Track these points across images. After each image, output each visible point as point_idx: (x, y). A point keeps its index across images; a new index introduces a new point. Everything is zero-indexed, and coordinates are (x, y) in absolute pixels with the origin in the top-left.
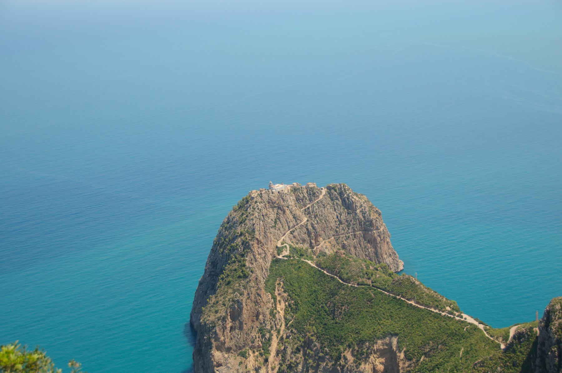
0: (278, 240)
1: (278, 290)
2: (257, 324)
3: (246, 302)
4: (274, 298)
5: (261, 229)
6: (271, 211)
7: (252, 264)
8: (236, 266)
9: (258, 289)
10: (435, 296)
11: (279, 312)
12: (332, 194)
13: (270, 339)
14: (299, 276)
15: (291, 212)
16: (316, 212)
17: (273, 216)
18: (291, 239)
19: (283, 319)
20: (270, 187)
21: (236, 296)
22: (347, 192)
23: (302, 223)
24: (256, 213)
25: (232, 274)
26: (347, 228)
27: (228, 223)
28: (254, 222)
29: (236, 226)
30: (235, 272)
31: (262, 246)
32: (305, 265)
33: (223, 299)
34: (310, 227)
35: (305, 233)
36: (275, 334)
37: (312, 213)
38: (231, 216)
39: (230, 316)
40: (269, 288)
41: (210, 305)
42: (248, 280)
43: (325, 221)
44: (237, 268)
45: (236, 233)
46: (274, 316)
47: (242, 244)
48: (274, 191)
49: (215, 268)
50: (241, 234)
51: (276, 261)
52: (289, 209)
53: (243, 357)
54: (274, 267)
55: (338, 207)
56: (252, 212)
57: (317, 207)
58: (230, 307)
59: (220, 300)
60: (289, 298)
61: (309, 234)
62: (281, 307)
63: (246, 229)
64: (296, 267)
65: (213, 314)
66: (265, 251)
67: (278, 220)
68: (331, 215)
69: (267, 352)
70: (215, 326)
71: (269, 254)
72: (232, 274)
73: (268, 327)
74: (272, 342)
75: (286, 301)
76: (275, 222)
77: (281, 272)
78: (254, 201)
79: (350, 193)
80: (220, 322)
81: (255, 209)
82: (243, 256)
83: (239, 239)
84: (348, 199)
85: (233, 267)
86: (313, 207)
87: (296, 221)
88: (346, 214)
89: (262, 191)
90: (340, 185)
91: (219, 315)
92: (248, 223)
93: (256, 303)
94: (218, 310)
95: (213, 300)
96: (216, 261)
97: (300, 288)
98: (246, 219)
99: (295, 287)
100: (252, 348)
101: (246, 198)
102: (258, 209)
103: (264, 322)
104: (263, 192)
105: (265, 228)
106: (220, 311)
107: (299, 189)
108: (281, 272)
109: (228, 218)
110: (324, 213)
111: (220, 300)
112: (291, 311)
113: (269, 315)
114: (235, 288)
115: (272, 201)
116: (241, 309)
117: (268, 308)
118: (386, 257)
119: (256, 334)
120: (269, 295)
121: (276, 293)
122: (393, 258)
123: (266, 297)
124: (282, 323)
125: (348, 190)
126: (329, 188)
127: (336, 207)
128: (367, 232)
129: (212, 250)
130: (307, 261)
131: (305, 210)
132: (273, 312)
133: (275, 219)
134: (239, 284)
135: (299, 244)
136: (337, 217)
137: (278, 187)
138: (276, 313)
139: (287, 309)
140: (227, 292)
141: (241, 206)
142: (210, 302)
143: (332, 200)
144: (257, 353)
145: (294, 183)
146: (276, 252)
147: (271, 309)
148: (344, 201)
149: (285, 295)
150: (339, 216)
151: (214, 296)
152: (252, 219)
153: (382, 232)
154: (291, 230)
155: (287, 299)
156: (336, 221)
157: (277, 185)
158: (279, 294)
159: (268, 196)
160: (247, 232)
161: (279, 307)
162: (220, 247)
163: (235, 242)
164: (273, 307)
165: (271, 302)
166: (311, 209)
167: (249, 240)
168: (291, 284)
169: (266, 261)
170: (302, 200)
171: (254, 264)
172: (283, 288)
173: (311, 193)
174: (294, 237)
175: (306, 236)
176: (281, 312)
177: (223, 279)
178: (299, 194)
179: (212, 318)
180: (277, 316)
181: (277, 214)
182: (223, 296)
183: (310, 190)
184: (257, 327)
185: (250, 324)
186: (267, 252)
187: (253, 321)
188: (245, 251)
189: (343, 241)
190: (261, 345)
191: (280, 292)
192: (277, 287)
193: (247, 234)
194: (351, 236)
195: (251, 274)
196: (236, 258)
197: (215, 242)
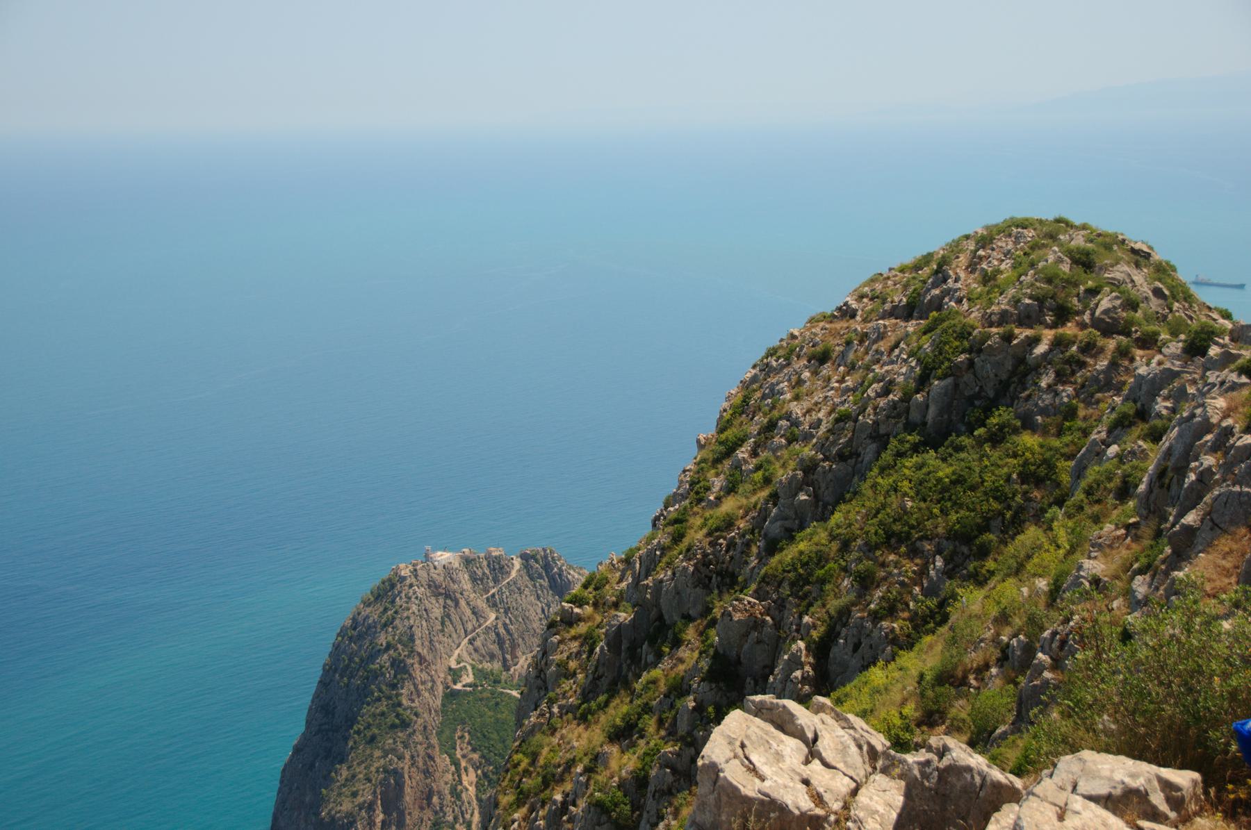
0: (450, 657)
1: (462, 749)
2: (428, 814)
4: (456, 763)
5: (424, 636)
6: (434, 602)
7: (413, 701)
8: (383, 706)
9: (428, 747)
11: (467, 790)
12: (532, 567)
14: (497, 720)
15: (468, 604)
16: (507, 603)
17: (437, 612)
18: (470, 654)
19: (475, 802)
20: (427, 557)
21: (390, 761)
23: (488, 623)
25: (377, 721)
27: (355, 629)
28: (412, 622)
29: (376, 632)
30: (383, 718)
31: (426, 668)
32: (506, 699)
33: (365, 769)
34: (502, 631)
35: (494, 642)
38: (359, 614)
39: (381, 799)
40: (445, 746)
41: (338, 784)
42: (410, 730)
43: (523, 620)
44: (385, 709)
45: (377, 644)
47: (392, 665)
48: (436, 563)
49: (330, 716)
50: (389, 647)
51: (451, 695)
54: (450, 706)
56: (405, 605)
57: (508, 594)
58: (380, 783)
59: (360, 773)
60: (483, 761)
61: (500, 642)
62: (469, 779)
63: (397, 637)
64: (491, 704)
65: (348, 799)
66: (431, 677)
67: (446, 619)
70: (355, 822)
71: (439, 683)
72: (377, 721)
73: (450, 818)
74: (799, 722)
75: (478, 768)
76: (443, 623)
77: (464, 715)
78: (408, 584)
79: (563, 565)
80: (363, 813)
81: (410, 598)
82: (394, 686)
83: (385, 657)
84: (560, 575)
85: (376, 708)
86: (502, 593)
87: (478, 620)
89: (417, 565)
90: (545, 550)
91: (360, 799)
92: (400, 626)
93: (427, 773)
94: (358, 791)
95: (345, 773)
96: (331, 704)
97: (504, 742)
98: (394, 619)
99: (493, 739)
101: (390, 580)
102: (417, 598)
103: (441, 808)
104: (418, 567)
105: (430, 633)
106: (361, 792)
107: (474, 560)
108: (464, 715)
109: (354, 619)
111: (360, 773)
112: (489, 785)
113: (449, 796)
114: (387, 747)
115: (434, 582)
116: (400, 785)
117: (446, 783)
121: (459, 754)
123: (443, 761)
124: (473, 809)
125: (559, 560)
126: (525, 557)
127: (539, 592)
129: (320, 682)
130: (509, 691)
131: (488, 599)
132: (456, 790)
134: (394, 739)
135: (484, 663)
136: (543, 611)
137: (443, 557)
138: (462, 792)
139: (482, 782)
140: (371, 756)
141: (379, 595)
142: (339, 778)
143: (532, 579)
145: (464, 550)
146: (450, 678)
147: (452, 785)
148: (554, 579)
149: (476, 756)
150: (546, 609)
151: (344, 767)
152: (408, 618)
154: (469, 637)
155: (480, 764)
156: (541, 619)
157: (439, 553)
158: (464, 756)
160: (400, 641)
162: (342, 676)
163: (378, 661)
164: (454, 780)
167: (405, 656)
168: (484, 736)
169: (434, 696)
170: (482, 580)
171: (416, 701)
172: (469, 743)
173: (497, 567)
174: (476, 650)
175: (495, 648)
176: (470, 788)
177: (358, 732)
178: (475, 569)
179: (347, 806)
180: (464, 795)
181: (444, 607)
182: (364, 765)
183: (494, 562)
184: (429, 819)
185: (416, 813)
186: (435, 678)
187: (422, 808)
188: (399, 677)
191: (465, 751)
192: (458, 744)
193: (399, 646)
195: (415, 718)
196: (380, 690)
197: (327, 667)
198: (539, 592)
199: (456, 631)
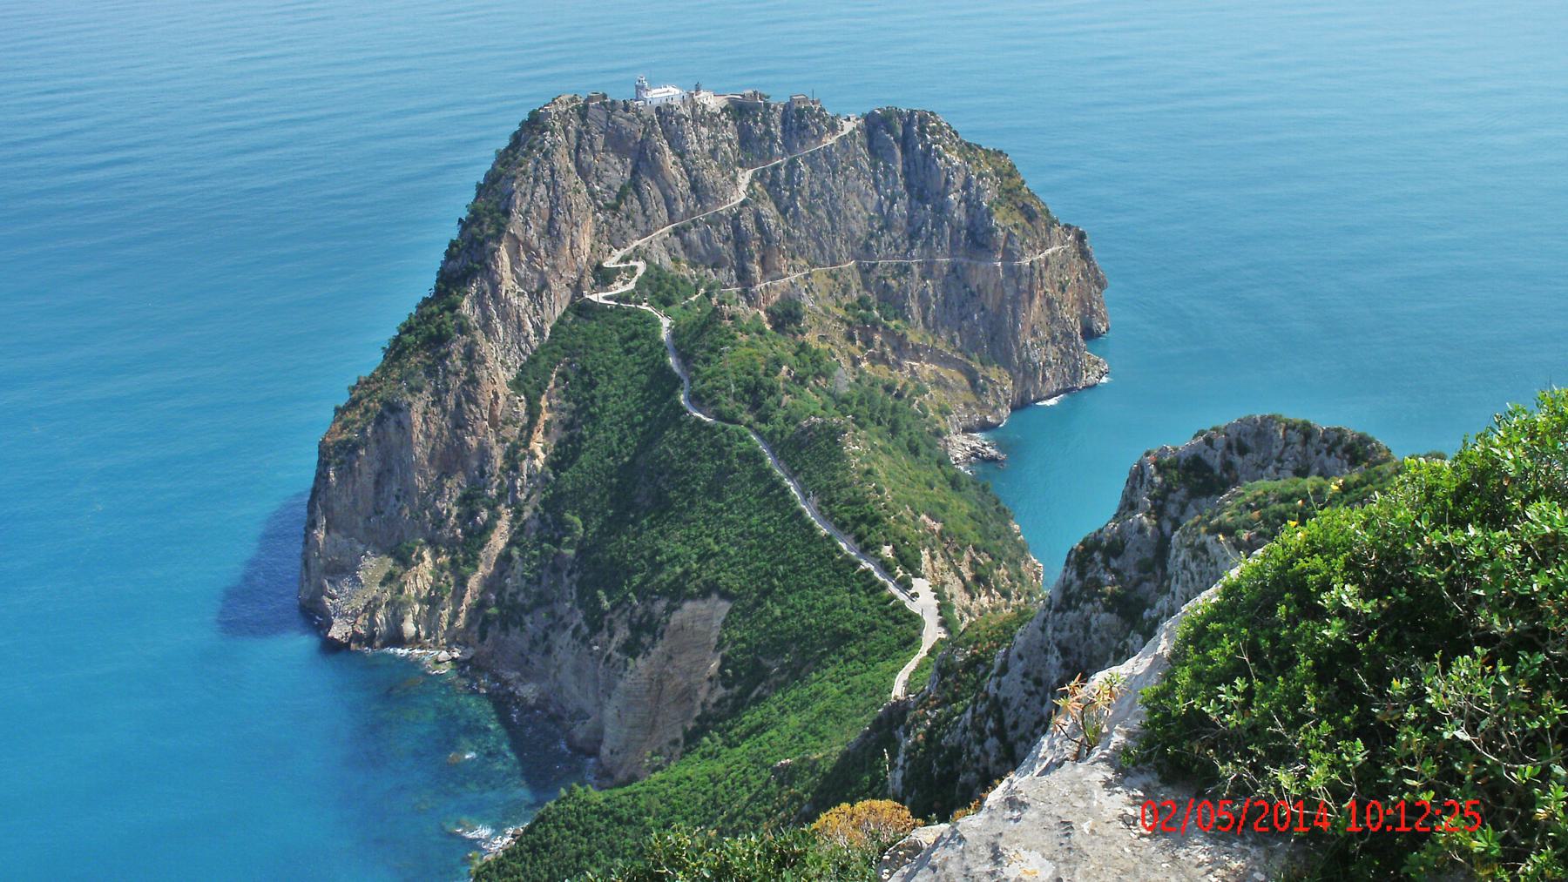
3: (426, 413)
4: (533, 413)
13: (489, 527)
22: (929, 137)
26: (907, 242)
36: (506, 515)
68: (858, 196)
69: (472, 562)
100: (432, 543)
118: (1032, 344)
120: (521, 401)
122: (1064, 350)
125: (931, 134)
133: (623, 188)
138: (524, 457)
144: (444, 559)
147: (513, 445)
153: (1026, 270)
156: (871, 218)
159: (609, 118)
161: (537, 444)
166: (783, 172)
175: (727, 250)
189: (885, 279)
194: (915, 268)
199: (644, 212)
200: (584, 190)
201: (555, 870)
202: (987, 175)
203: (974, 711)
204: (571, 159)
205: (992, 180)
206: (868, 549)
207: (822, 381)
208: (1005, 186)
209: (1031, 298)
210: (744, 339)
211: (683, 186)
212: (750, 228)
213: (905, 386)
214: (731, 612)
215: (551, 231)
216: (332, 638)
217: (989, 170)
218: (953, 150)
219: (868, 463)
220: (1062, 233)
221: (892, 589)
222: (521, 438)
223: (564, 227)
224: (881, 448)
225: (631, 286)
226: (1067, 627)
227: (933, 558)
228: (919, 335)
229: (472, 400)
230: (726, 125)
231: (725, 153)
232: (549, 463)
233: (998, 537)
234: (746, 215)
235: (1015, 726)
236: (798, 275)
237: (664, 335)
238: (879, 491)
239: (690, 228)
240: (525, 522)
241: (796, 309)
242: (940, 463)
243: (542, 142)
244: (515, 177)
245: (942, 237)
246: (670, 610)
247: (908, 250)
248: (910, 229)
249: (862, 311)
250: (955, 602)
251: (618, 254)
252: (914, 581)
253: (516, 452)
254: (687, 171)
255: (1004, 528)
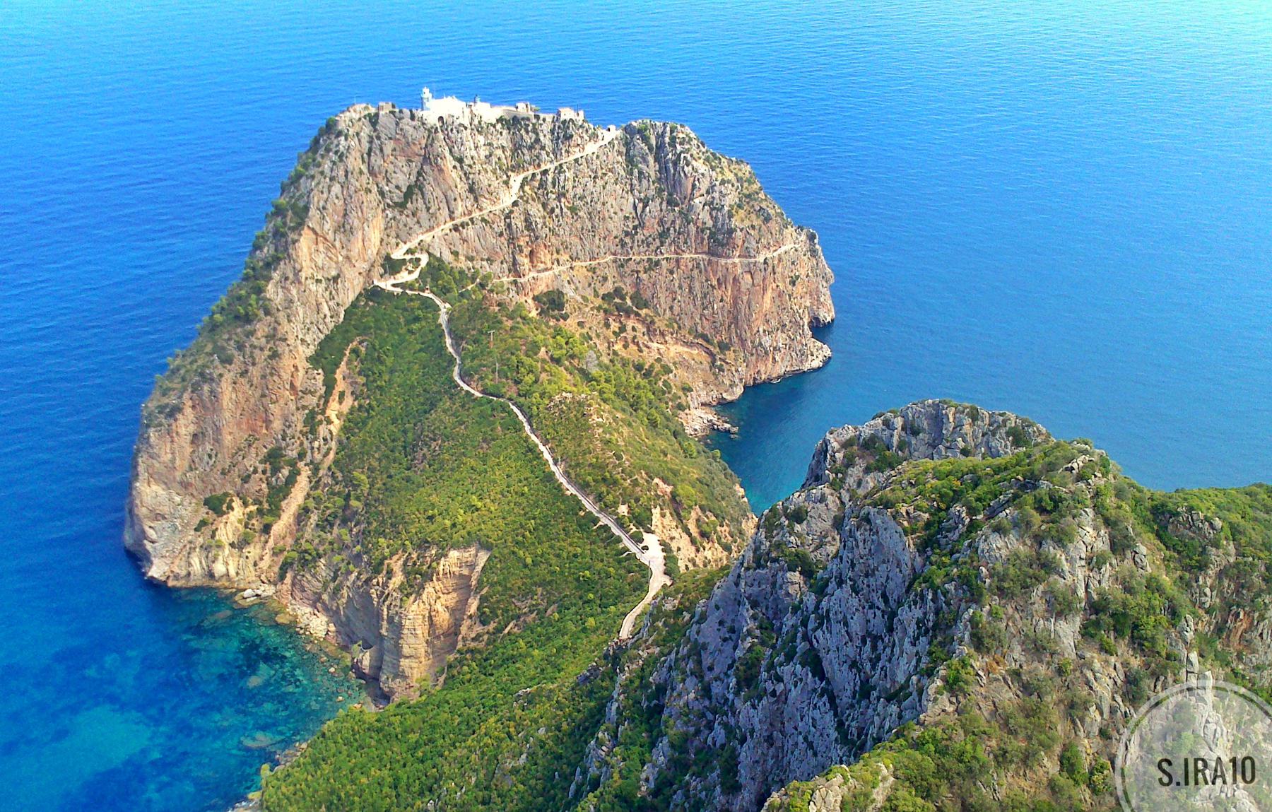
4: (330, 384)
10: (610, 467)
13: (291, 481)
24: (328, 162)
26: (657, 240)
34: (518, 222)
37: (554, 187)
46: (313, 431)
52: (462, 168)
53: (213, 510)
55: (640, 182)
67: (416, 190)
69: (276, 511)
84: (675, 164)
88: (661, 204)
110: (592, 193)
119: (257, 464)
124: (330, 449)
125: (681, 144)
127: (635, 182)
128: (714, 259)
133: (409, 187)
137: (436, 108)
138: (321, 422)
159: (397, 124)
161: (333, 410)
165: (318, 394)
189: (638, 272)
190: (266, 490)
198: (635, 182)
199: (428, 209)
200: (374, 189)
201: (332, 781)
202: (729, 181)
203: (677, 653)
204: (363, 161)
205: (733, 185)
206: (607, 508)
207: (575, 362)
208: (745, 191)
209: (764, 290)
210: (509, 323)
211: (462, 187)
212: (519, 226)
213: (652, 366)
214: (489, 559)
215: (343, 228)
216: (152, 577)
217: (731, 177)
218: (700, 158)
219: (611, 434)
220: (794, 234)
221: (627, 543)
222: (318, 405)
223: (356, 223)
224: (622, 420)
225: (416, 275)
226: (756, 583)
227: (663, 516)
228: (665, 322)
229: (274, 371)
230: (501, 133)
231: (499, 159)
232: (344, 429)
233: (723, 499)
234: (516, 214)
235: (711, 669)
236: (561, 268)
237: (443, 319)
238: (619, 457)
239: (468, 225)
240: (320, 478)
241: (559, 298)
242: (675, 434)
243: (337, 145)
244: (313, 177)
245: (688, 235)
246: (438, 557)
247: (658, 248)
248: (660, 229)
249: (617, 300)
250: (681, 555)
251: (404, 248)
252: (646, 536)
253: (313, 418)
254: (465, 174)
255: (728, 491)
